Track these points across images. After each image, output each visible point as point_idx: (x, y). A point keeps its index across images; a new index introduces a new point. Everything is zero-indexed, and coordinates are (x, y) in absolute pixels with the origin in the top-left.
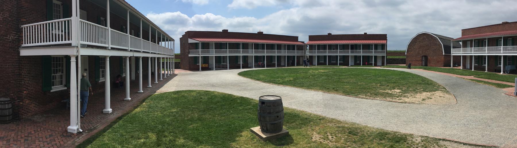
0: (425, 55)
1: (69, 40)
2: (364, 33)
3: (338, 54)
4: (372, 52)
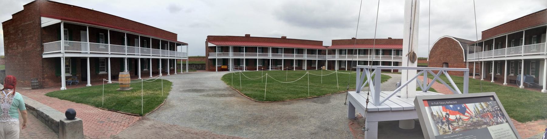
3: (258, 57)
4: (316, 57)
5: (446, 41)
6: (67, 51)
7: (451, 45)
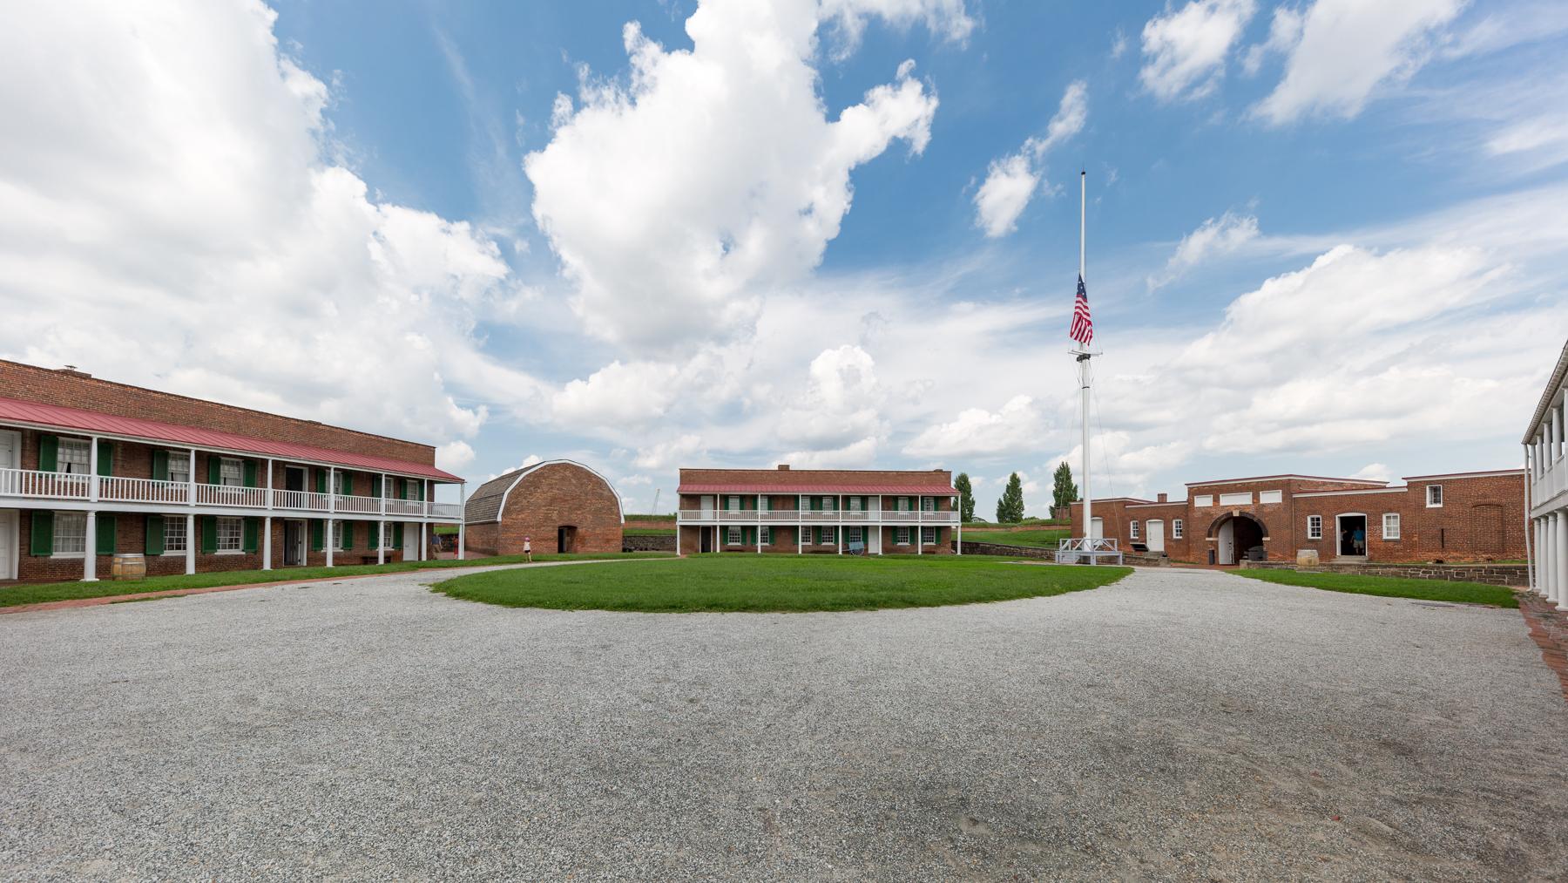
6: (275, 507)
7: (582, 484)
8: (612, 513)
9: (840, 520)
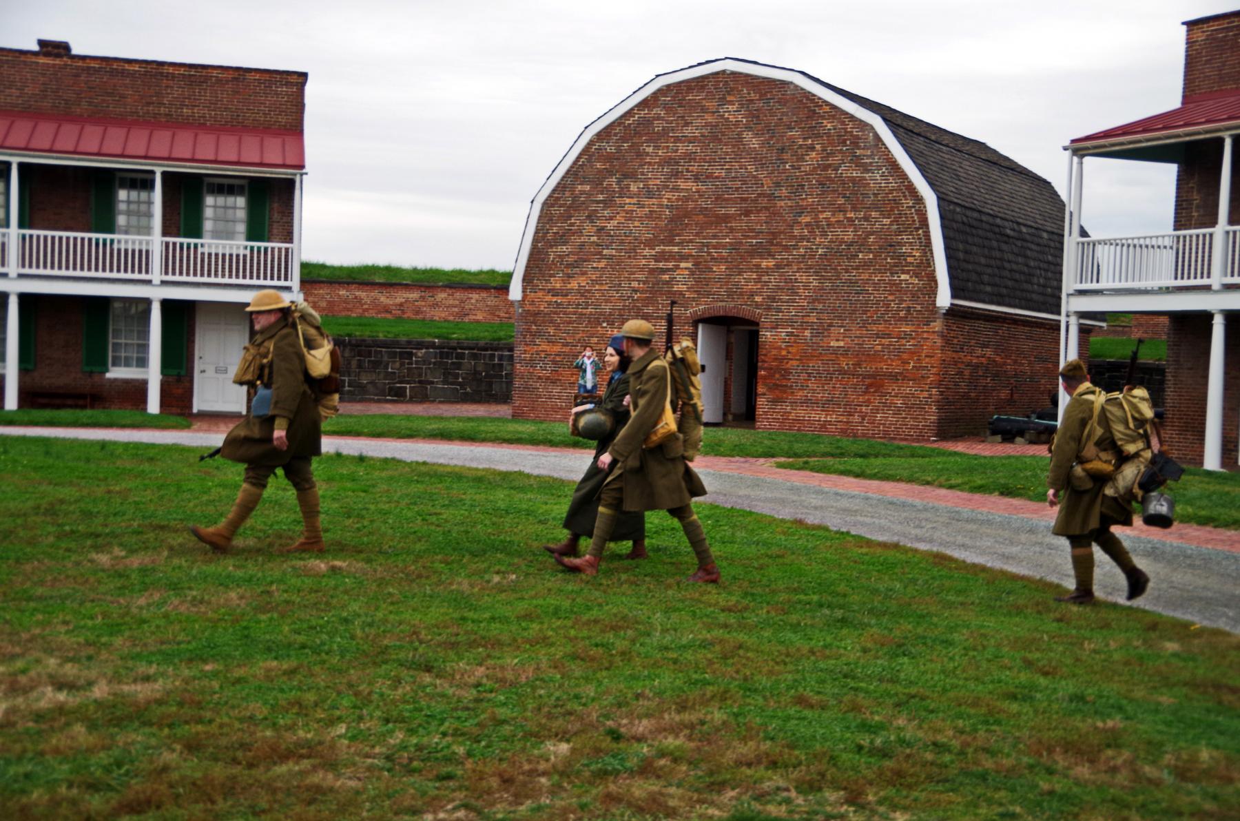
0: (724, 306)
1: (286, 279)
2: (42, 43)
5: (732, 112)
8: (900, 264)
9: (1216, 280)
